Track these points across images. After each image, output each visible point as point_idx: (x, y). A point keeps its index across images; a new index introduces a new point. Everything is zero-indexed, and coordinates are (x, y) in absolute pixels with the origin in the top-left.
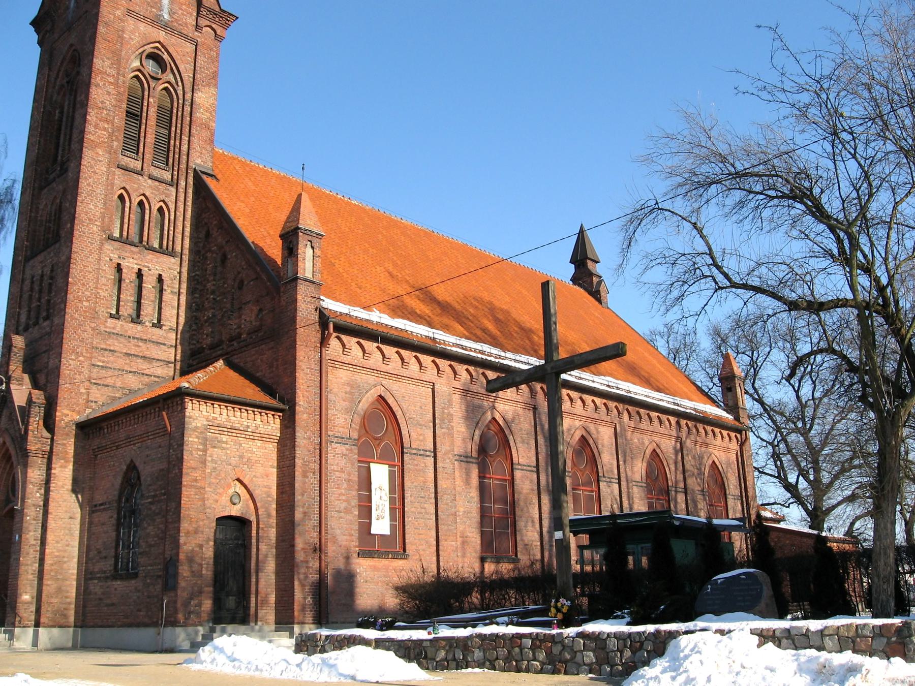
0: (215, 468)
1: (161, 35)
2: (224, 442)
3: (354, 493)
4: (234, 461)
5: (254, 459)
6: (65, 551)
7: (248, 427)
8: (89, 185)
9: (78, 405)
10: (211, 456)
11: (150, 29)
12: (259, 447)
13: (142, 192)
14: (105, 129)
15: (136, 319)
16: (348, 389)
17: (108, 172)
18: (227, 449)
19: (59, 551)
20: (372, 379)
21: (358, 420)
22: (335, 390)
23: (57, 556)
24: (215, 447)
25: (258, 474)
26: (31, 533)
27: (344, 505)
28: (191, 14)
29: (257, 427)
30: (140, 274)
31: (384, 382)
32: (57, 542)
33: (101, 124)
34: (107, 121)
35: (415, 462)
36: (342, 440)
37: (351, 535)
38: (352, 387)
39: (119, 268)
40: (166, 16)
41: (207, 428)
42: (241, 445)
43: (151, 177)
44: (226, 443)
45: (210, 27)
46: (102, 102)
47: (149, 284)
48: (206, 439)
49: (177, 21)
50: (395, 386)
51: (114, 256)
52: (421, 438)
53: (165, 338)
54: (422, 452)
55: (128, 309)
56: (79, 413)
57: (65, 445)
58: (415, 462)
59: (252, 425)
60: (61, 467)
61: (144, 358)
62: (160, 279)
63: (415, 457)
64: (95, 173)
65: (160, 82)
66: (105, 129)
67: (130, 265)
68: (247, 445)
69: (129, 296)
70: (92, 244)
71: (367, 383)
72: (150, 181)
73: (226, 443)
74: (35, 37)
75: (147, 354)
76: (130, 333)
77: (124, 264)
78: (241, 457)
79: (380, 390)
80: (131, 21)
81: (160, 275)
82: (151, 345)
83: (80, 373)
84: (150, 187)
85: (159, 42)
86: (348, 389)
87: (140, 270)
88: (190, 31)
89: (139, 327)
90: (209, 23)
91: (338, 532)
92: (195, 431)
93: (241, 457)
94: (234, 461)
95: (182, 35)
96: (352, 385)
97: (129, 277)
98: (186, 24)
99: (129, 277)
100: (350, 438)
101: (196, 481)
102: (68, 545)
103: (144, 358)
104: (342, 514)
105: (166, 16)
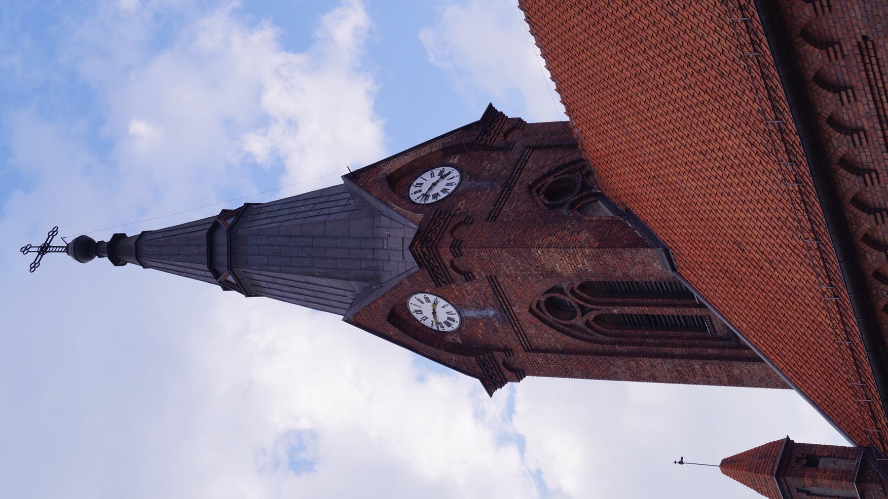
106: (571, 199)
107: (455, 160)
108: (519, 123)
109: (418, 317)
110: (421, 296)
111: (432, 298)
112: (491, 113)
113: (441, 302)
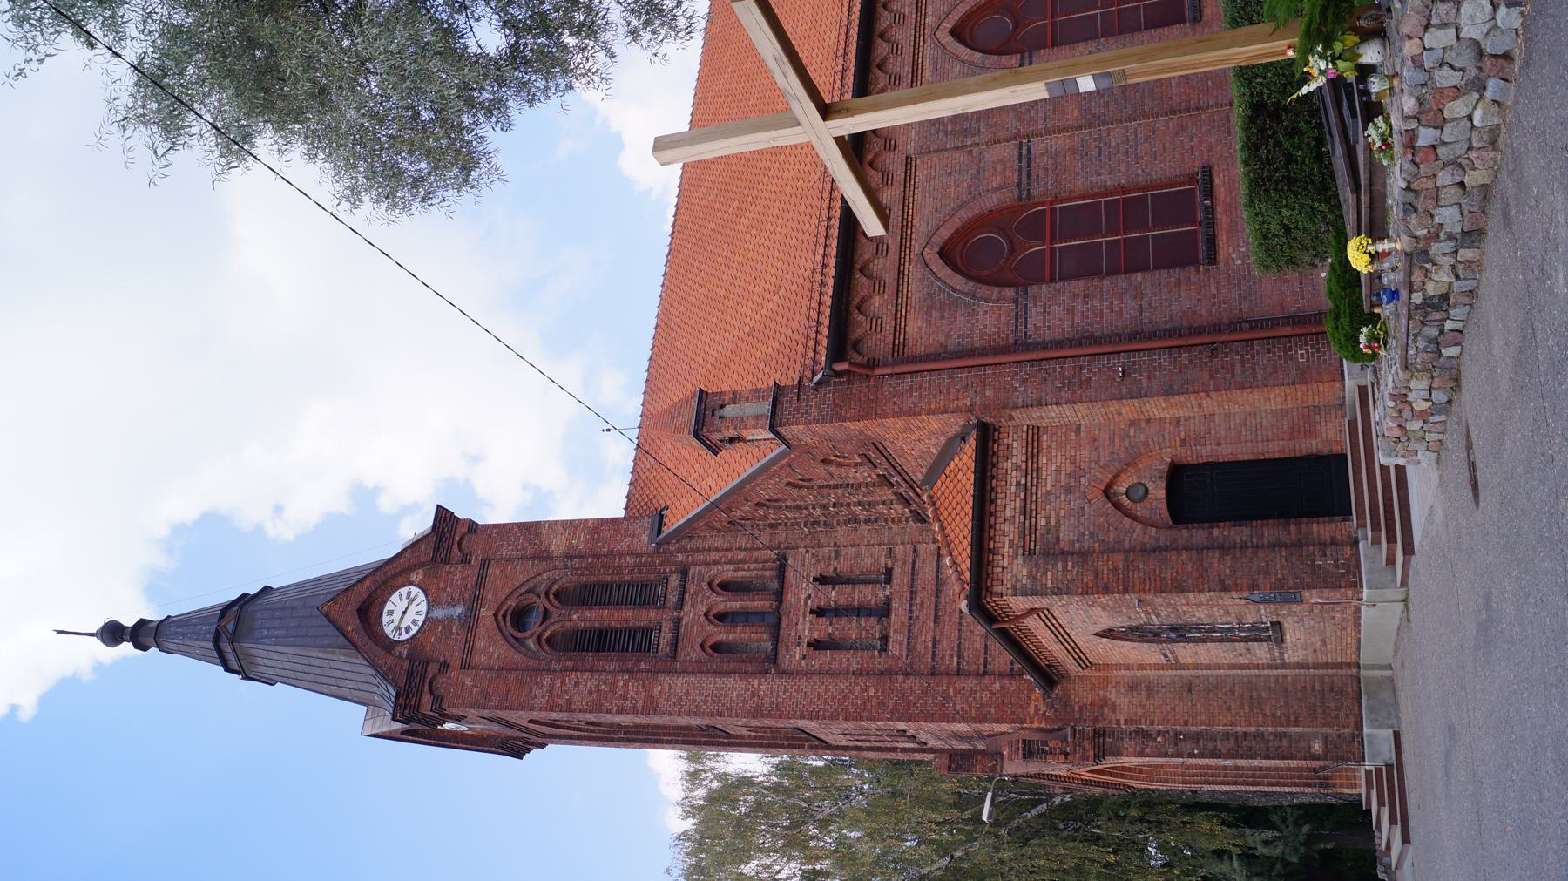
0: (1092, 535)
1: (486, 613)
2: (1048, 523)
3: (1106, 282)
4: (1076, 502)
5: (1067, 467)
6: (1242, 696)
7: (1018, 483)
8: (705, 702)
9: (1020, 692)
10: (1072, 543)
11: (481, 631)
12: (1049, 459)
13: (702, 618)
14: (625, 685)
15: (884, 611)
16: (936, 314)
17: (684, 672)
18: (1058, 515)
19: (1242, 706)
20: (915, 272)
21: (983, 290)
22: (941, 337)
23: (1251, 709)
24: (1058, 538)
25: (1094, 456)
26: (1219, 746)
27: (1127, 300)
28: (448, 573)
29: (1017, 468)
30: (819, 612)
31: (917, 248)
32: (1229, 709)
33: (620, 692)
34: (614, 684)
35: (1042, 173)
36: (1020, 316)
37: (1179, 282)
38: (931, 308)
39: (816, 645)
40: (459, 610)
41: (1029, 554)
42: (1049, 492)
43: (680, 605)
44: (1048, 518)
45: (460, 544)
46: (590, 693)
47: (833, 595)
48: (1046, 554)
49: (462, 594)
50: (921, 227)
51: (798, 653)
52: (999, 167)
53: (904, 563)
54: (1024, 164)
55: (872, 626)
56: (1031, 691)
57: (1081, 708)
58: (1042, 173)
59: (1014, 477)
60: (1114, 711)
61: (938, 592)
62: (821, 580)
63: (1033, 177)
64: (687, 694)
65: (548, 606)
66: (625, 685)
67: (805, 627)
68: (1048, 484)
69: (851, 628)
70: (786, 690)
71: (921, 280)
72: (686, 608)
73: (1048, 518)
74: (536, 752)
75: (931, 588)
76: (905, 619)
77: (806, 635)
78: (1068, 490)
79: (931, 255)
80: (476, 660)
81: (815, 579)
82: (919, 585)
83: (973, 692)
84: (693, 606)
85: (495, 615)
86: (936, 314)
87: (812, 612)
88: (472, 573)
89: (895, 604)
90: (455, 546)
91: (1175, 308)
92: (1035, 578)
93: (1068, 490)
94: (1076, 502)
95: (479, 584)
96: (930, 304)
97: (824, 628)
98: (463, 579)
99: (824, 628)
100: (1016, 301)
101: (1115, 569)
102: (1233, 693)
103: (938, 592)
104: (1145, 305)
105: (459, 610)
107: (416, 576)
108: (472, 526)
112: (444, 517)
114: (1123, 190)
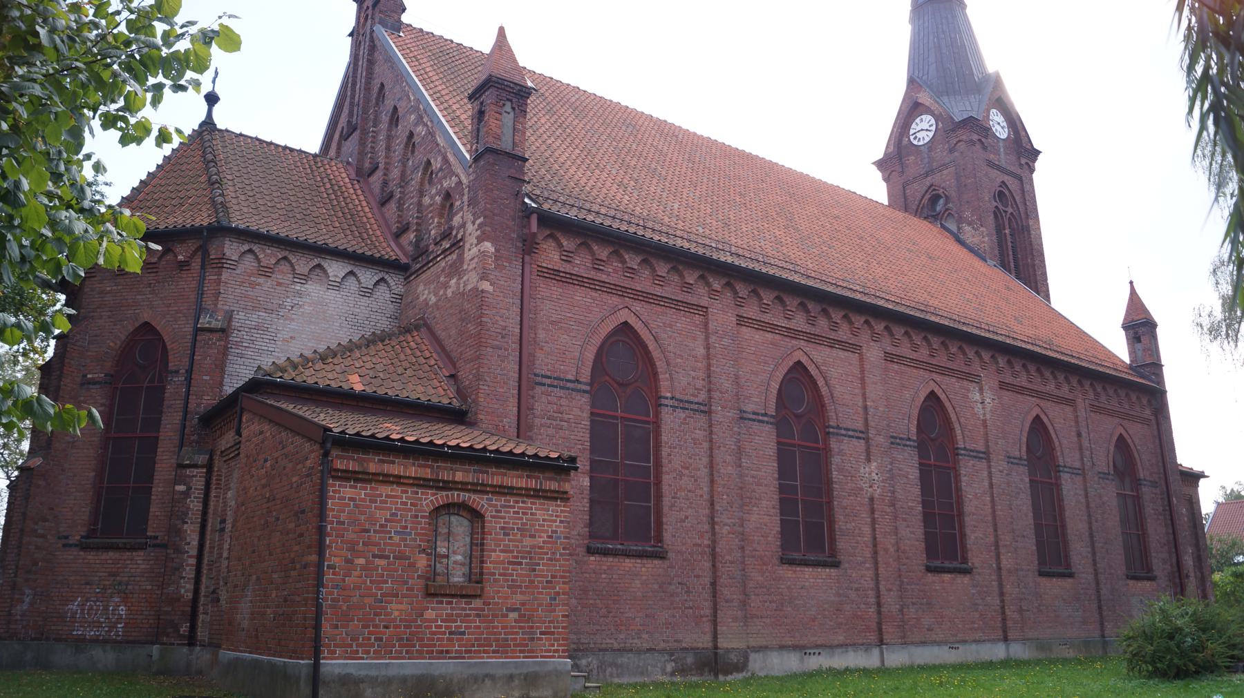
106: (1000, 207)
108: (1032, 170)
109: (918, 120)
110: (933, 121)
111: (933, 128)
113: (931, 134)
114: (658, 483)
